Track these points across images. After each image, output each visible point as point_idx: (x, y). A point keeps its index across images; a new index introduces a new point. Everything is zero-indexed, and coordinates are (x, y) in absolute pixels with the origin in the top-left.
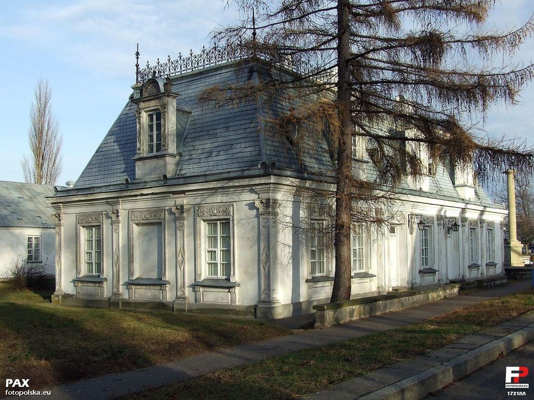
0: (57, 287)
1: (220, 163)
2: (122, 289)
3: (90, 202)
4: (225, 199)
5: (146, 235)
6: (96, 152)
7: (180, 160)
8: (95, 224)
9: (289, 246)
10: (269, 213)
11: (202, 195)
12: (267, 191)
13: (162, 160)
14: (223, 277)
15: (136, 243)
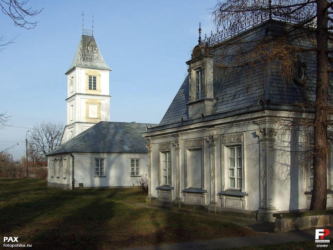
0: (149, 193)
1: (241, 102)
2: (181, 195)
3: (163, 136)
4: (239, 130)
5: (195, 157)
6: (173, 101)
7: (217, 103)
8: (237, 144)
9: (287, 165)
10: (266, 139)
11: (224, 128)
12: (265, 123)
13: (203, 103)
14: (238, 188)
15: (189, 163)
